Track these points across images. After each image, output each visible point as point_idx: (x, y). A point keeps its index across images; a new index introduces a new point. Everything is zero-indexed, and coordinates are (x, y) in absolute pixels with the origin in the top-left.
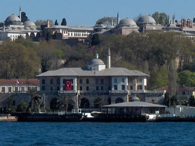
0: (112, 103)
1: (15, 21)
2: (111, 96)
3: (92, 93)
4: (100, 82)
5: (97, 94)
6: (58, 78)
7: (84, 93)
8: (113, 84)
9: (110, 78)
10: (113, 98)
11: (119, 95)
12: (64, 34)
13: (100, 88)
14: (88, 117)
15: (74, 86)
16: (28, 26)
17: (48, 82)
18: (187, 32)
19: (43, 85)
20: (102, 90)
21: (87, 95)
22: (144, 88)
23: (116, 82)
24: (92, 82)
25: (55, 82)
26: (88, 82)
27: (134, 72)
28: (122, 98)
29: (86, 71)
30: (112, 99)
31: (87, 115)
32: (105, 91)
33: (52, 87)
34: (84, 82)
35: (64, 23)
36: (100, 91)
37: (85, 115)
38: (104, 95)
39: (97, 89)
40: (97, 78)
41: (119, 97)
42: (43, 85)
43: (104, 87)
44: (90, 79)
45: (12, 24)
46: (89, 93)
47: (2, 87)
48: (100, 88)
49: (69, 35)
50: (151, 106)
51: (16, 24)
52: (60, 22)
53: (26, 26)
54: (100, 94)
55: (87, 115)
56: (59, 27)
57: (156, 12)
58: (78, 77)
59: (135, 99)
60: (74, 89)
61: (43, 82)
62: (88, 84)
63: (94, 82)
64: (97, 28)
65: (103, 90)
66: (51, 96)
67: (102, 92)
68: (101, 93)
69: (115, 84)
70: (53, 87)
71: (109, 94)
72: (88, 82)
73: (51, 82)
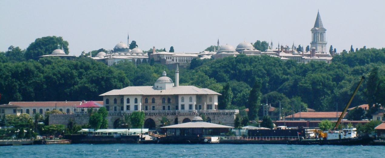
0: (178, 123)
2: (178, 116)
3: (158, 113)
4: (166, 101)
5: (163, 114)
6: (122, 97)
7: (173, 113)
8: (180, 103)
9: (176, 97)
10: (180, 119)
11: (187, 115)
12: (168, 60)
13: (166, 108)
14: (146, 139)
15: (213, 105)
16: (135, 53)
17: (112, 101)
18: (283, 56)
19: (107, 105)
20: (168, 110)
21: (152, 116)
22: (214, 107)
23: (183, 100)
24: (158, 101)
25: (119, 101)
26: (153, 101)
27: (204, 90)
28: (275, 108)
29: (156, 91)
30: (179, 120)
31: (145, 137)
32: (172, 111)
33: (35, 109)
34: (150, 101)
35: (172, 50)
36: (167, 111)
37: (143, 137)
38: (171, 115)
39: (164, 108)
40: (163, 97)
42: (107, 105)
43: (170, 107)
44: (156, 98)
46: (155, 113)
47: (271, 106)
48: (166, 108)
50: (215, 127)
52: (168, 49)
53: (133, 53)
54: (166, 114)
55: (145, 137)
56: (164, 54)
57: (258, 41)
58: (143, 96)
60: (138, 109)
61: (107, 102)
62: (154, 104)
63: (161, 101)
64: (200, 54)
65: (170, 110)
66: (114, 116)
67: (168, 112)
68: (167, 113)
69: (183, 103)
70: (117, 106)
71: (176, 114)
72: (136, 101)
73: (115, 101)
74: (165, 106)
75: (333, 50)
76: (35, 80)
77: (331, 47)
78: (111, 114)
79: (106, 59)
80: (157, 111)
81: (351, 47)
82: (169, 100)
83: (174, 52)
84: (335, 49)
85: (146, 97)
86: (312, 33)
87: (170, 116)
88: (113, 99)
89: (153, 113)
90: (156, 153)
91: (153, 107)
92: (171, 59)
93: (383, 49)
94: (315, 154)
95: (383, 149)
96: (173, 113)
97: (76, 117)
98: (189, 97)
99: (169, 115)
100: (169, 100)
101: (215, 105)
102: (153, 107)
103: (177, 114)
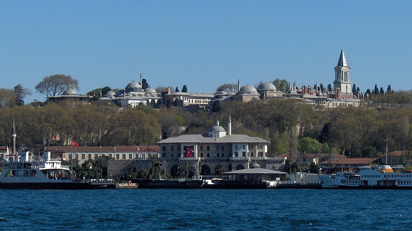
1: (136, 88)
2: (231, 163)
6: (179, 144)
8: (234, 150)
10: (234, 165)
11: (240, 162)
13: (220, 155)
16: (149, 93)
17: (168, 149)
18: (308, 98)
19: (164, 152)
23: (236, 148)
24: (213, 148)
25: (175, 149)
26: (208, 149)
27: (255, 138)
34: (205, 148)
35: (185, 89)
36: (221, 158)
38: (225, 161)
41: (240, 163)
42: (164, 152)
44: (210, 146)
45: (132, 91)
48: (220, 155)
49: (190, 102)
51: (136, 91)
52: (180, 89)
53: (147, 93)
54: (221, 161)
58: (198, 144)
59: (255, 166)
64: (217, 95)
65: (224, 157)
68: (221, 160)
69: (236, 151)
70: (174, 153)
71: (230, 161)
72: (208, 149)
73: (172, 149)
74: (243, 156)
75: (356, 89)
76: (66, 125)
77: (354, 86)
78: (168, 161)
79: (118, 99)
80: (212, 158)
81: (375, 87)
82: (223, 147)
83: (187, 92)
84: (358, 89)
85: (201, 145)
86: (336, 72)
87: (224, 162)
88: (170, 146)
89: (208, 160)
90: (134, 195)
91: (208, 154)
92: (187, 100)
93: (411, 91)
94: (294, 198)
95: (347, 191)
96: (226, 160)
97: (136, 163)
98: (242, 145)
99: (223, 162)
100: (223, 147)
101: (266, 153)
102: (208, 154)
103: (231, 161)
